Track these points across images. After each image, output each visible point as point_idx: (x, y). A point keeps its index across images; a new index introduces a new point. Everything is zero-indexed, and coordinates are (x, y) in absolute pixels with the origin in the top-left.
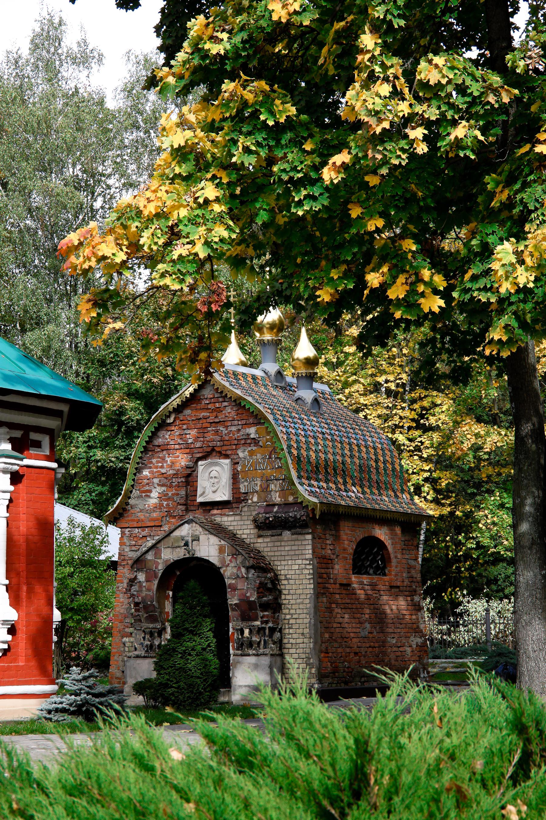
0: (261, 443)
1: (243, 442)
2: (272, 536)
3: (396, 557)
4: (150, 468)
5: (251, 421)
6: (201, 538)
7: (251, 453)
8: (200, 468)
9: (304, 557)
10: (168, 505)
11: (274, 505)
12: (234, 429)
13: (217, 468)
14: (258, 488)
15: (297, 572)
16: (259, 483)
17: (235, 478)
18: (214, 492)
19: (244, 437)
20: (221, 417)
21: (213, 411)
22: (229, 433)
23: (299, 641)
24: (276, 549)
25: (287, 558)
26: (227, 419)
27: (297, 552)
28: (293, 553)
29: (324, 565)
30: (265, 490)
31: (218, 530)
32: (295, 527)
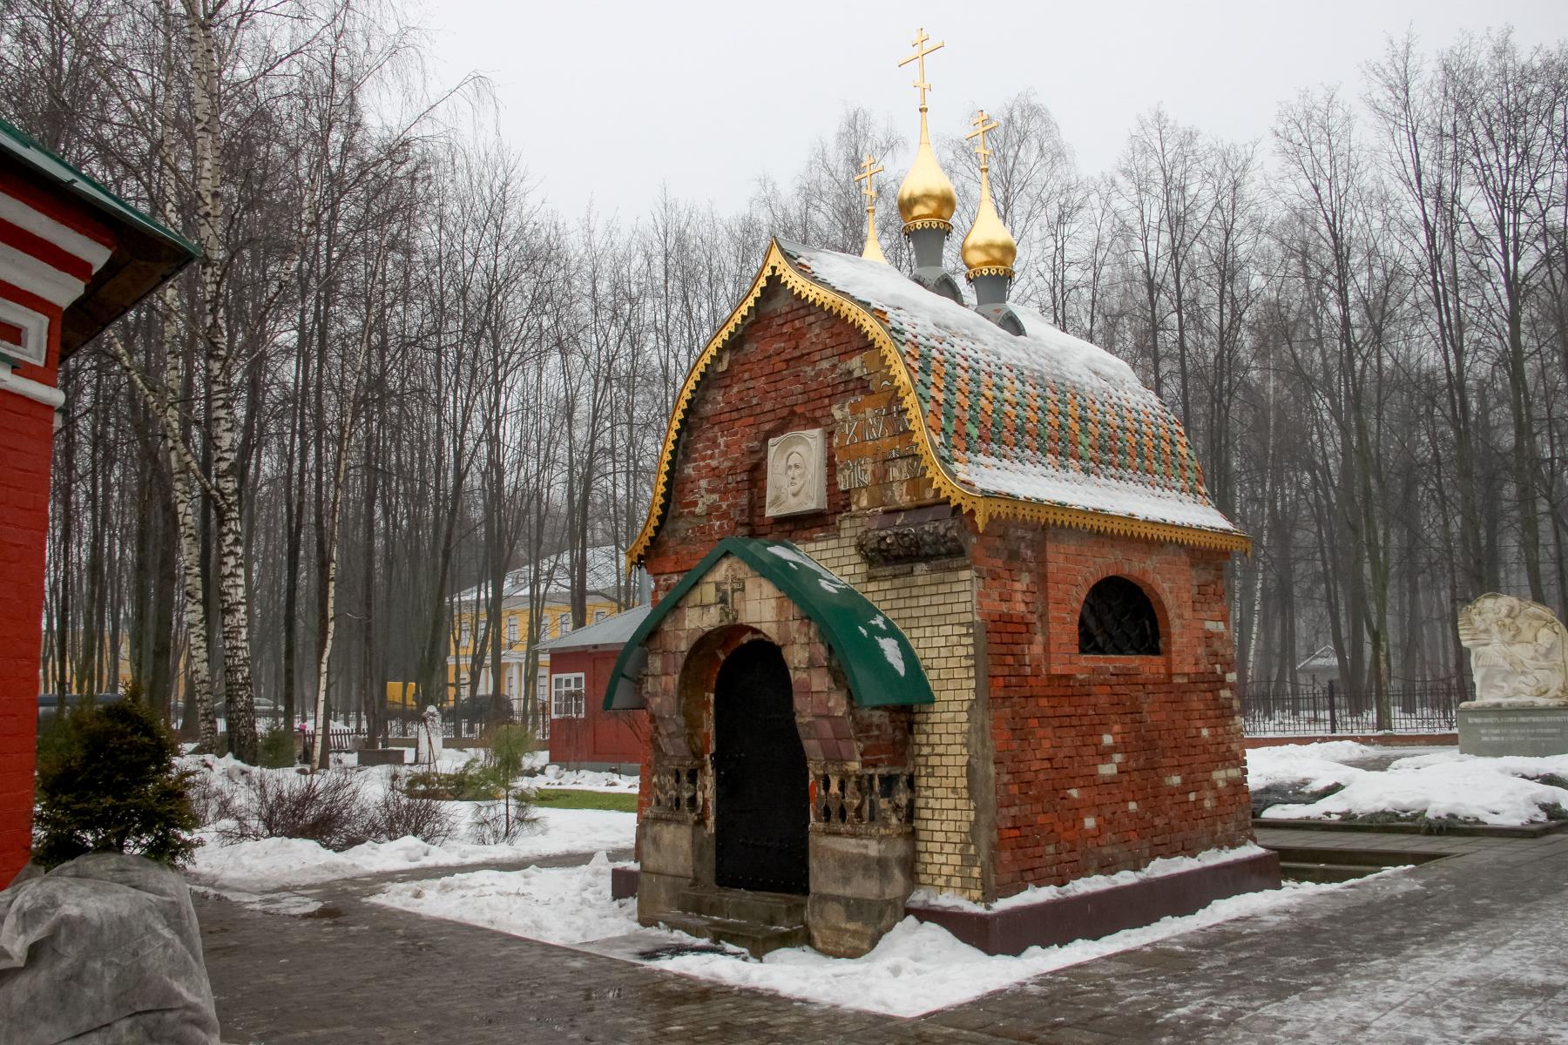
0: (872, 387)
1: (841, 388)
2: (895, 576)
3: (1180, 616)
4: (695, 460)
5: (855, 345)
6: (748, 585)
7: (856, 409)
8: (772, 451)
9: (955, 619)
10: (721, 527)
11: (898, 511)
12: (825, 365)
13: (800, 448)
14: (867, 479)
15: (944, 653)
16: (870, 468)
17: (831, 467)
18: (795, 495)
19: (844, 378)
20: (805, 346)
21: (790, 337)
22: (817, 375)
23: (949, 804)
24: (901, 603)
25: (923, 622)
26: (814, 348)
27: (942, 610)
28: (934, 611)
29: (1006, 638)
30: (882, 480)
31: (778, 574)
32: (937, 556)
